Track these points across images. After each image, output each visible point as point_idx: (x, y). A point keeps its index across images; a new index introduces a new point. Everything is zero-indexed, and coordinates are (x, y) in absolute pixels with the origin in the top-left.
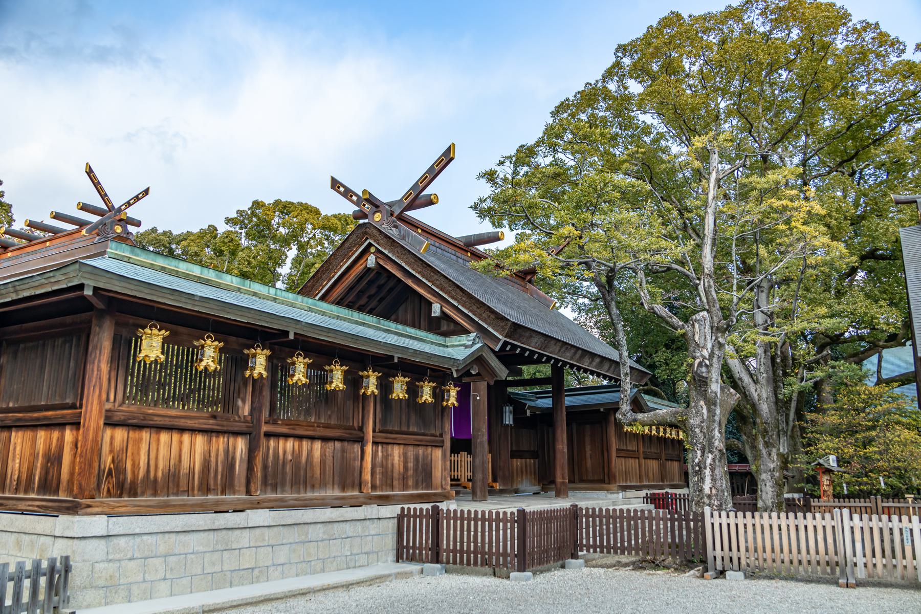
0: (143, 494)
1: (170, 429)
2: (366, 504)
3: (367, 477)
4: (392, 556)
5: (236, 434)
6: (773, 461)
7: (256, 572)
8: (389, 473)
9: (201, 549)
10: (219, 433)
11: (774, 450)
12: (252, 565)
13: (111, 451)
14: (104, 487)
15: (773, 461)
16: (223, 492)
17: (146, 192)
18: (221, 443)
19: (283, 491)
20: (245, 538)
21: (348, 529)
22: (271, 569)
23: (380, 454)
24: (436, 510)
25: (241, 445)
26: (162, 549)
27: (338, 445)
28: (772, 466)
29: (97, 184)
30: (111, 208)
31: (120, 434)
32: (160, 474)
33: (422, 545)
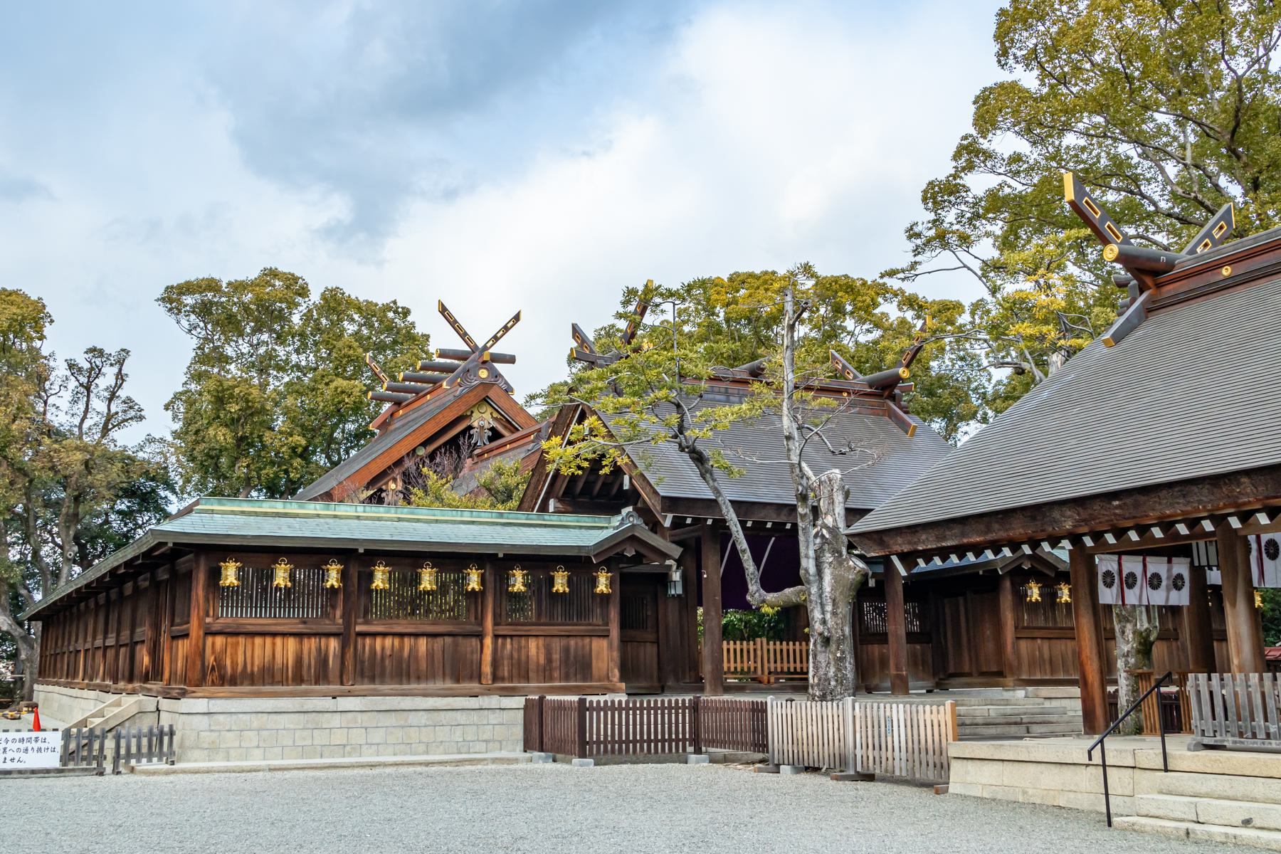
0: (242, 684)
1: (263, 634)
2: (483, 694)
3: (487, 669)
4: (521, 746)
5: (328, 635)
6: (1128, 642)
7: (348, 748)
8: (523, 665)
9: (292, 726)
10: (309, 635)
11: (1129, 627)
12: (344, 742)
13: (213, 652)
14: (209, 678)
15: (1128, 642)
16: (317, 683)
17: (517, 318)
18: (311, 644)
19: (409, 683)
20: (336, 720)
21: (461, 717)
22: (364, 747)
23: (509, 646)
24: (582, 702)
25: (333, 644)
26: (255, 725)
27: (448, 640)
28: (1126, 648)
29: (453, 323)
30: (474, 348)
31: (219, 640)
32: (256, 669)
33: (541, 735)
